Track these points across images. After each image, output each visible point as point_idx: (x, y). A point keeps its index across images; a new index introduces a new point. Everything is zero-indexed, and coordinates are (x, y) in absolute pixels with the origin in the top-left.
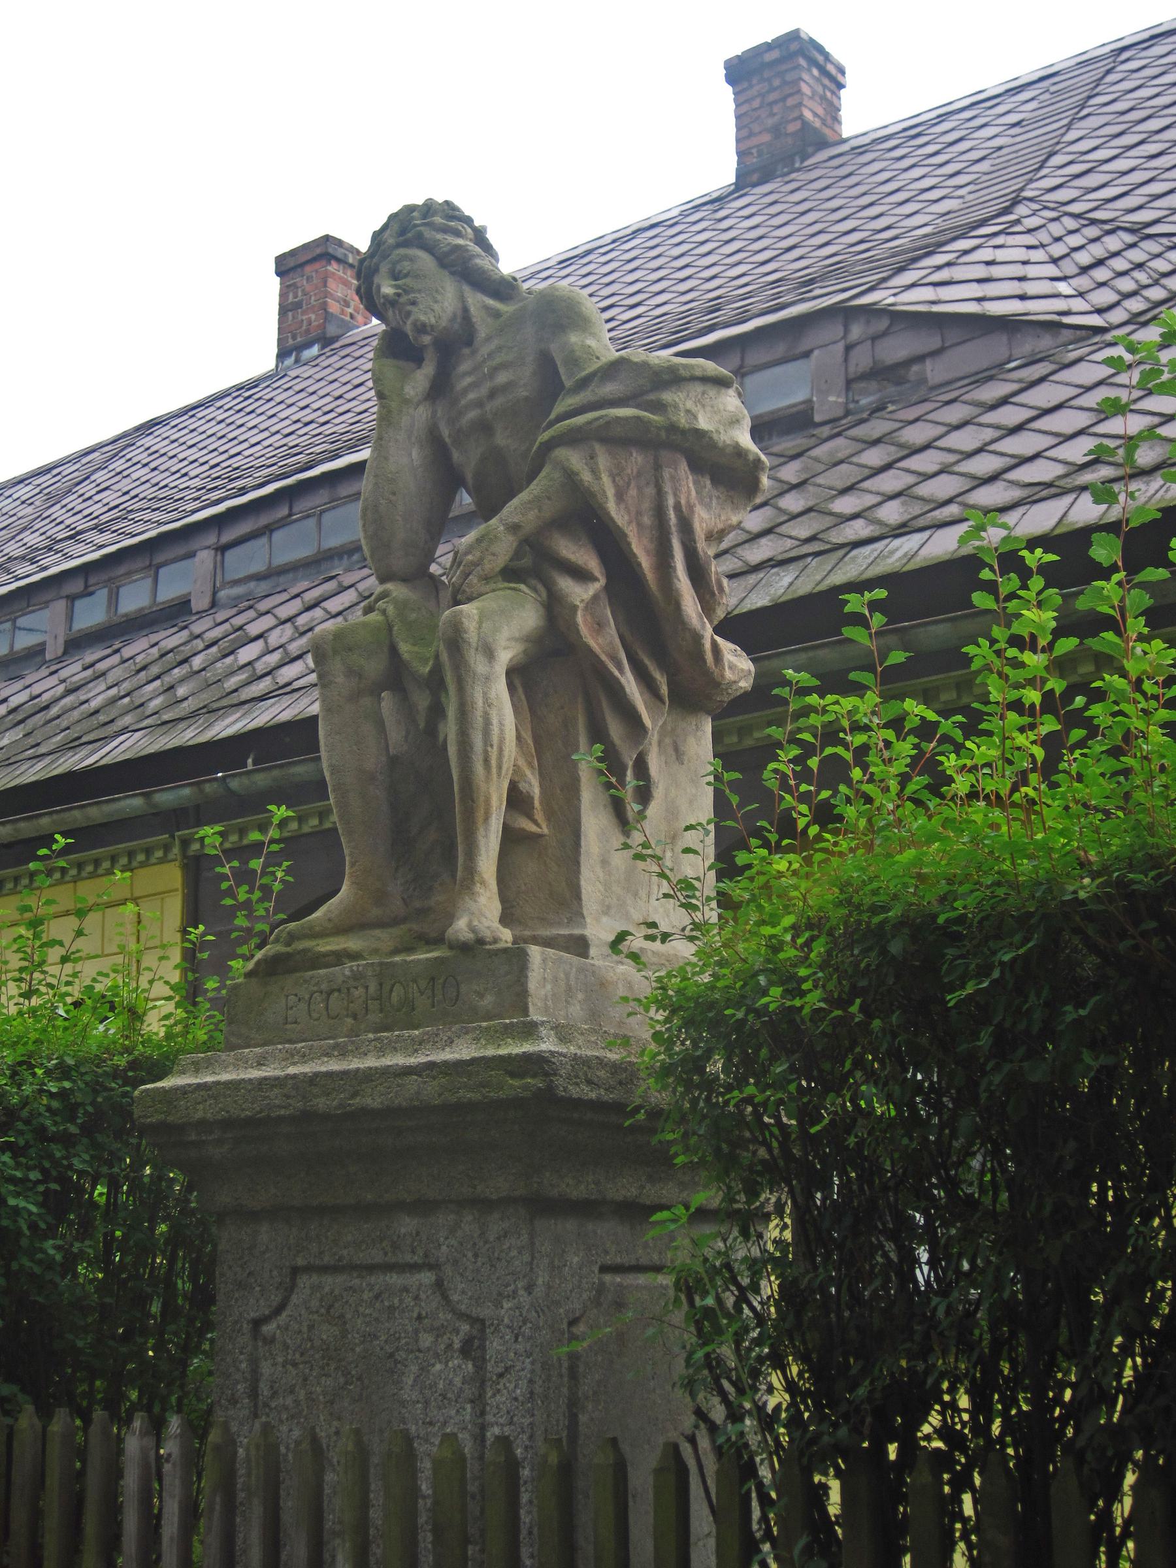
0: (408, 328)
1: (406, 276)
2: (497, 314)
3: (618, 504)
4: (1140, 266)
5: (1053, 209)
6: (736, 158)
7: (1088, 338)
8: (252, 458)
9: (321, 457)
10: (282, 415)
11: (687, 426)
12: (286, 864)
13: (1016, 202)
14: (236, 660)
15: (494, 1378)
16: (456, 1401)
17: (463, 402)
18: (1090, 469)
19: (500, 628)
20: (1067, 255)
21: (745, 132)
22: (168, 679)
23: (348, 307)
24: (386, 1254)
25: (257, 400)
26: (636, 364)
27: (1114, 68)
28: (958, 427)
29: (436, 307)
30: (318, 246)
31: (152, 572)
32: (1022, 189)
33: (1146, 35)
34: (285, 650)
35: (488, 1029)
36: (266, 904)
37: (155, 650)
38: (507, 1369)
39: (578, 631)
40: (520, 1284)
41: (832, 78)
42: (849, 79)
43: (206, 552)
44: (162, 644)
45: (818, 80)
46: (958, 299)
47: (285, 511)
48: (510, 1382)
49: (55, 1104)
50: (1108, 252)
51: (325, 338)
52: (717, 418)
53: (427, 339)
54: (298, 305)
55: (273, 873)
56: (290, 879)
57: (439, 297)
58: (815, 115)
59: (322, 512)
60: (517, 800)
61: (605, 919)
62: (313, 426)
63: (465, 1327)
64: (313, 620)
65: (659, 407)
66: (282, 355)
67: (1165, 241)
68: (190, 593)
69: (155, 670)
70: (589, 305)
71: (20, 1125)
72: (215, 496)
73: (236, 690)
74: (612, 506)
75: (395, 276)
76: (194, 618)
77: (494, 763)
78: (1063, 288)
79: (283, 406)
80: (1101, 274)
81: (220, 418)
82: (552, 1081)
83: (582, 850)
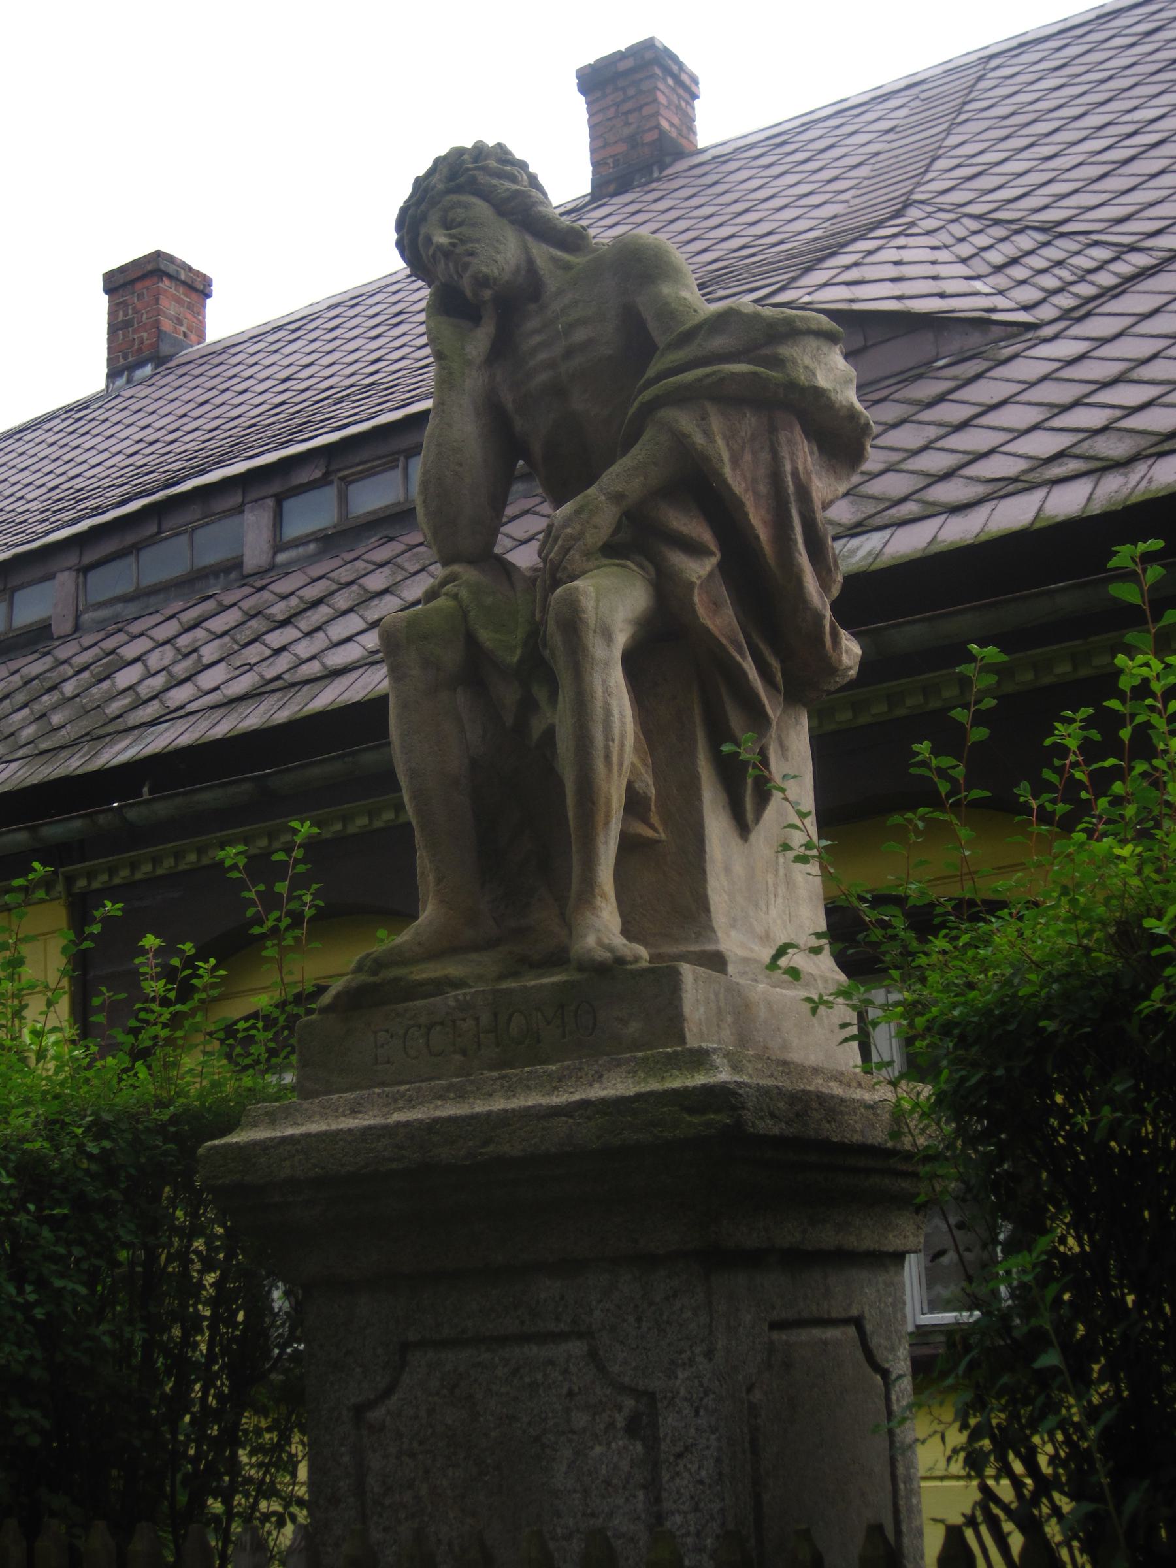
0: (466, 283)
1: (460, 224)
2: (567, 267)
3: (733, 469)
4: (1059, 263)
5: (949, 211)
6: (590, 168)
7: (1020, 335)
8: (95, 480)
9: (182, 474)
10: (122, 435)
11: (806, 383)
12: (315, 886)
13: (907, 205)
14: (114, 685)
15: (672, 1459)
16: (624, 1488)
17: (532, 363)
18: (1056, 463)
19: (613, 605)
20: (976, 255)
21: (600, 143)
22: (37, 707)
23: (181, 325)
24: (522, 1323)
25: (90, 421)
26: (747, 315)
27: (984, 75)
28: (894, 426)
29: (499, 258)
30: (149, 262)
31: (7, 596)
32: (911, 192)
33: (1014, 43)
34: (169, 673)
35: (644, 1060)
36: (297, 932)
37: (16, 678)
38: (687, 1448)
39: (694, 611)
40: (698, 1350)
41: (686, 88)
42: (703, 89)
43: (66, 574)
44: (24, 671)
45: (673, 90)
46: (876, 297)
47: (153, 529)
48: (691, 1462)
49: (94, 1167)
50: (1021, 250)
51: (158, 358)
52: (832, 377)
53: (487, 294)
54: (127, 325)
55: (300, 897)
56: (321, 903)
57: (501, 247)
58: (672, 124)
59: (194, 529)
60: (635, 804)
61: (733, 933)
62: (159, 445)
63: (629, 1403)
64: (195, 641)
65: (778, 362)
66: (112, 375)
67: (1081, 238)
68: (50, 618)
69: (20, 698)
70: (677, 253)
71: (56, 1193)
72: (66, 516)
73: (120, 716)
74: (727, 471)
75: (447, 225)
76: (56, 643)
77: (615, 759)
78: (978, 285)
79: (120, 427)
80: (1018, 272)
81: (50, 441)
82: (741, 1116)
83: (707, 856)
